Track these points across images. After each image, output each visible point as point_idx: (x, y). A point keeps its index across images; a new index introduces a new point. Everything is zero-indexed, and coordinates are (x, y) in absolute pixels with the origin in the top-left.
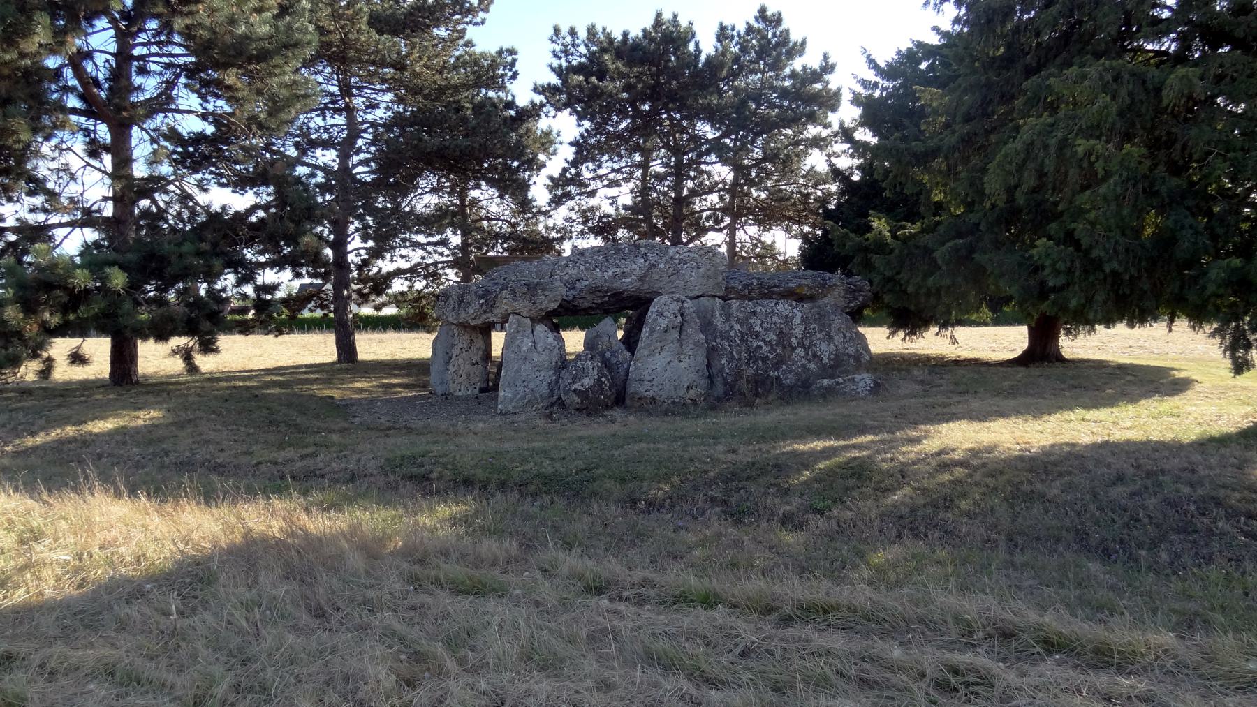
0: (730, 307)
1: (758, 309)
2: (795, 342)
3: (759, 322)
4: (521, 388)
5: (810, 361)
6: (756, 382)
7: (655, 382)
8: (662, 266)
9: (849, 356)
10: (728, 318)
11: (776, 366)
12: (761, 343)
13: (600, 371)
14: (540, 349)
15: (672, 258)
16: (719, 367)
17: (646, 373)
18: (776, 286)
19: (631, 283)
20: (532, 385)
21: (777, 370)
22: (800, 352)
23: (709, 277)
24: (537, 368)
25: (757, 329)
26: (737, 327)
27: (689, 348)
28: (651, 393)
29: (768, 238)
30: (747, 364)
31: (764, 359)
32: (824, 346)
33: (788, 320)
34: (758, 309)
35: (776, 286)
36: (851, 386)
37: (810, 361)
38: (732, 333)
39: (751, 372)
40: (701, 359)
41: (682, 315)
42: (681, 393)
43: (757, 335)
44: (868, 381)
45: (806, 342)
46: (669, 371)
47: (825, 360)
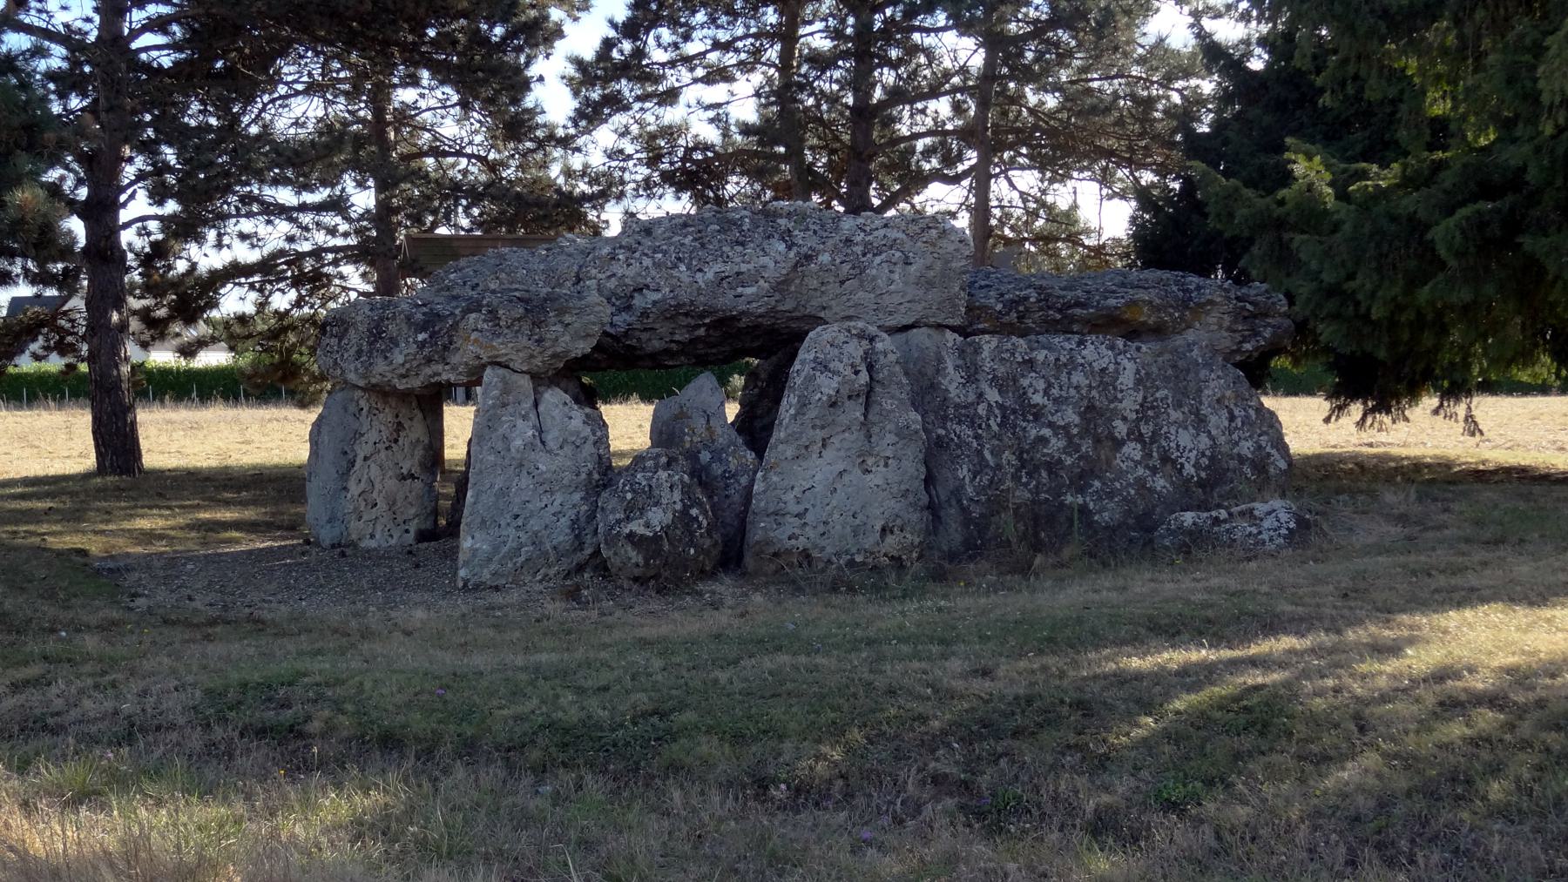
0: (977, 350)
1: (1040, 356)
2: (1121, 428)
3: (1041, 385)
4: (512, 531)
5: (1154, 470)
6: (1036, 519)
7: (809, 518)
8: (825, 258)
9: (1241, 459)
10: (971, 374)
11: (1080, 482)
12: (1046, 432)
13: (687, 491)
14: (552, 444)
15: (848, 241)
16: (952, 484)
17: (790, 497)
18: (1078, 304)
19: (757, 297)
20: (535, 525)
21: (1081, 490)
22: (1133, 450)
23: (930, 284)
24: (547, 486)
25: (1038, 399)
26: (993, 396)
27: (886, 443)
28: (801, 543)
29: (1060, 197)
30: (1016, 478)
31: (1053, 466)
32: (1185, 438)
33: (1106, 380)
34: (1040, 356)
35: (1078, 304)
36: (1244, 527)
37: (1154, 470)
38: (982, 410)
39: (1022, 495)
40: (911, 467)
41: (870, 368)
42: (869, 542)
43: (1038, 415)
44: (1284, 517)
45: (1146, 430)
46: (840, 494)
47: (1189, 469)
